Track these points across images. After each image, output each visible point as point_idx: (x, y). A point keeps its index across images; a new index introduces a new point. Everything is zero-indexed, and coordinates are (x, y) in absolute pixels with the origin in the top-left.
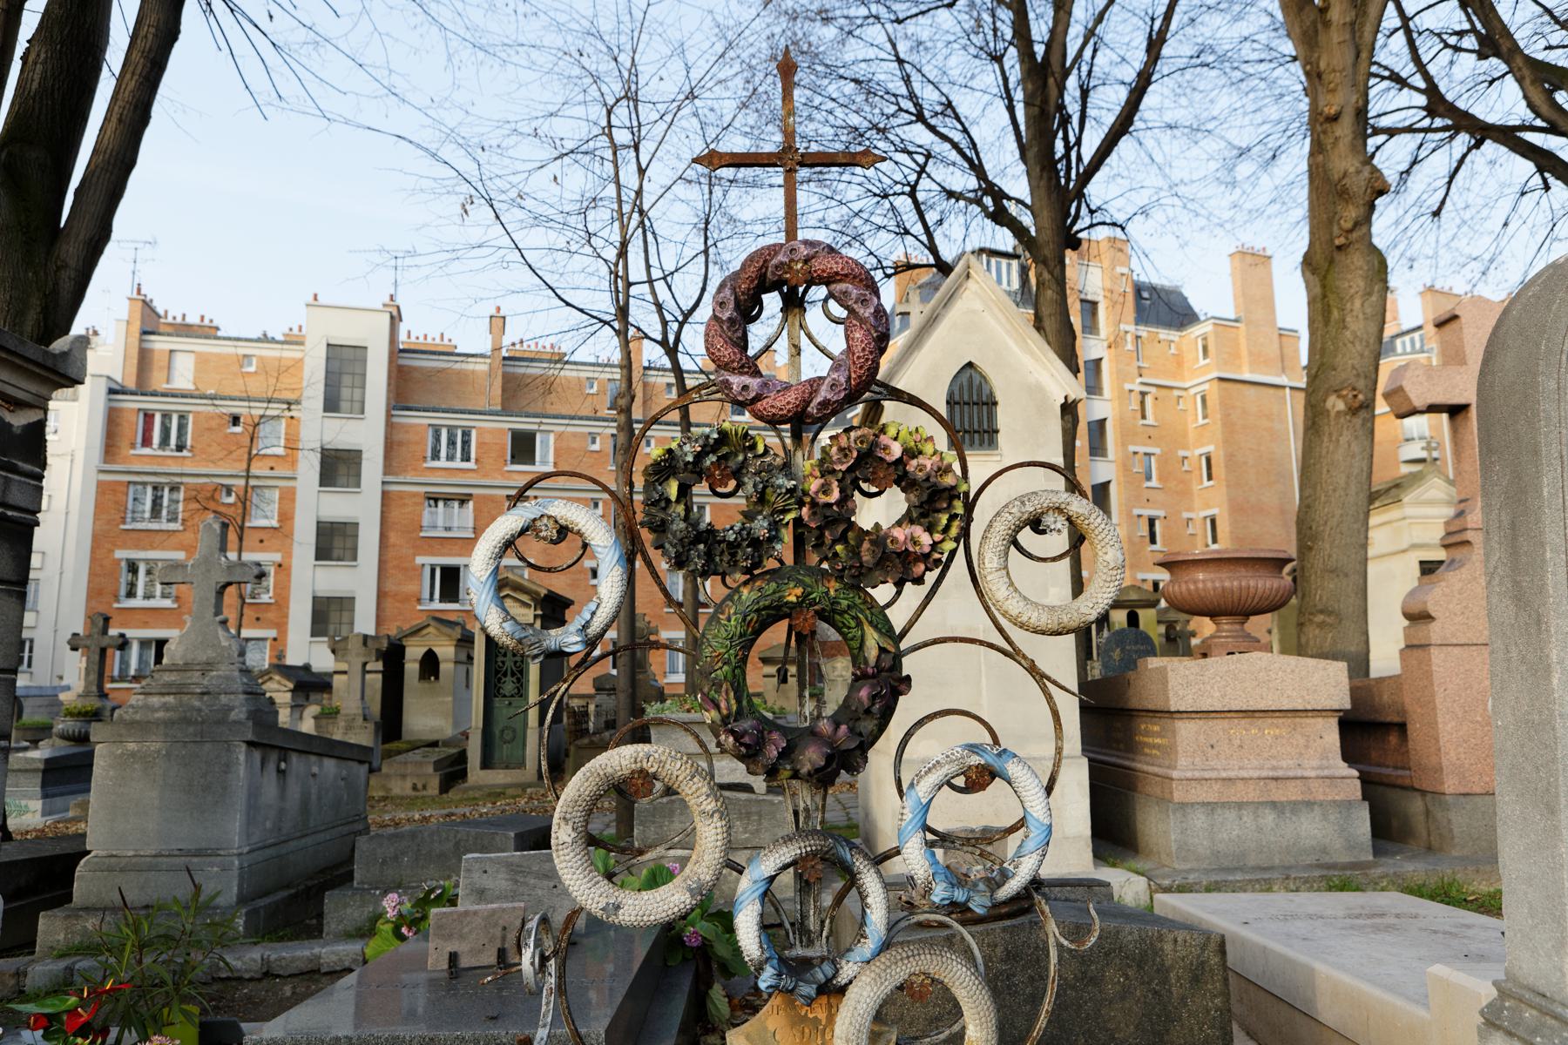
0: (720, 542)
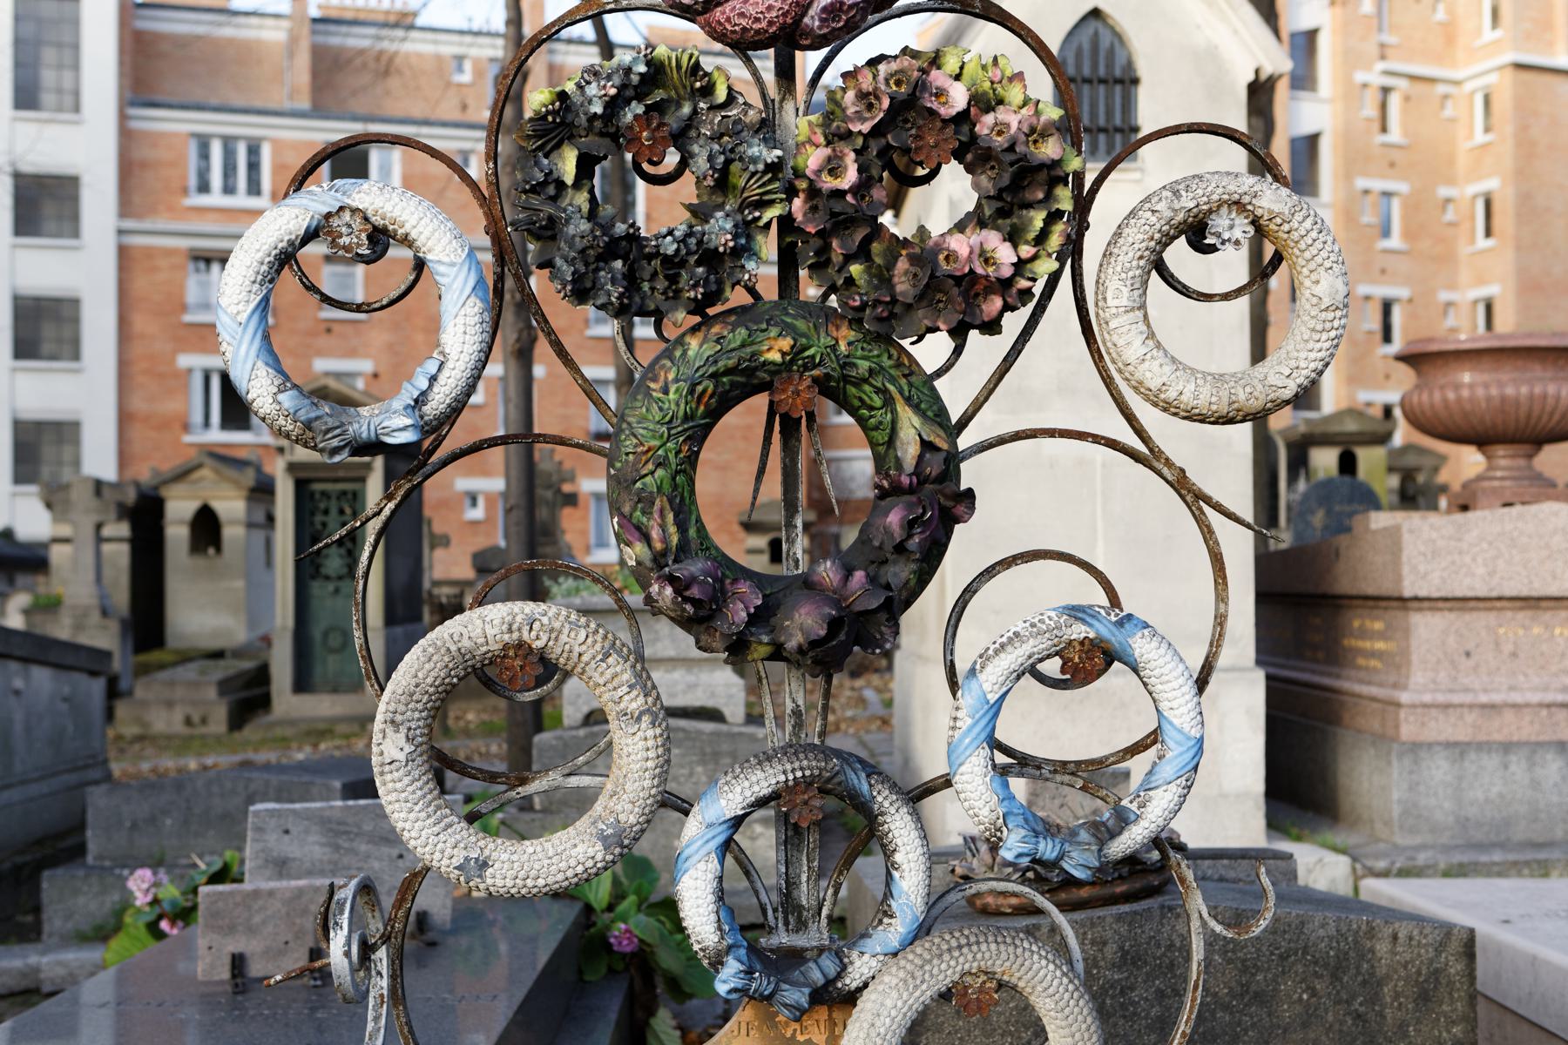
0: (650, 257)
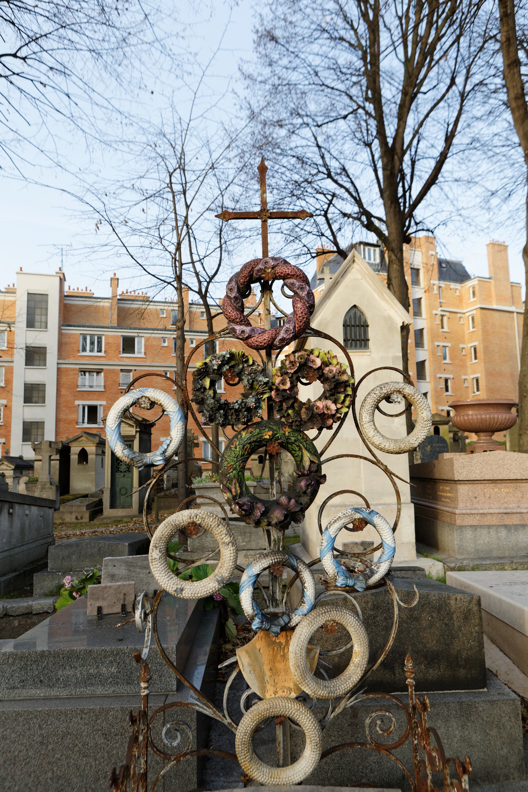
0: (231, 409)
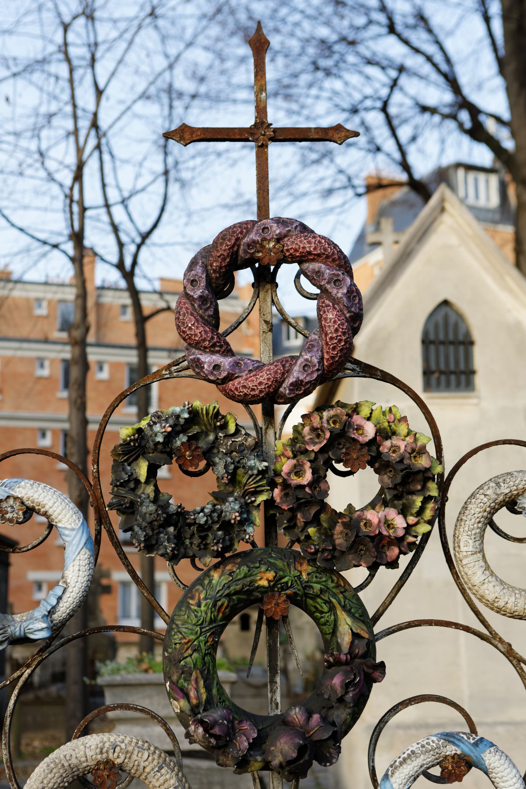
0: (190, 525)
